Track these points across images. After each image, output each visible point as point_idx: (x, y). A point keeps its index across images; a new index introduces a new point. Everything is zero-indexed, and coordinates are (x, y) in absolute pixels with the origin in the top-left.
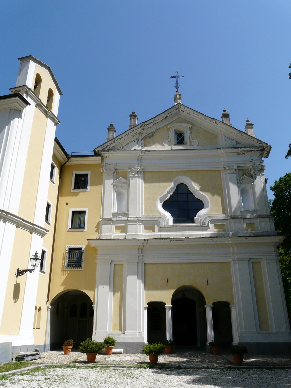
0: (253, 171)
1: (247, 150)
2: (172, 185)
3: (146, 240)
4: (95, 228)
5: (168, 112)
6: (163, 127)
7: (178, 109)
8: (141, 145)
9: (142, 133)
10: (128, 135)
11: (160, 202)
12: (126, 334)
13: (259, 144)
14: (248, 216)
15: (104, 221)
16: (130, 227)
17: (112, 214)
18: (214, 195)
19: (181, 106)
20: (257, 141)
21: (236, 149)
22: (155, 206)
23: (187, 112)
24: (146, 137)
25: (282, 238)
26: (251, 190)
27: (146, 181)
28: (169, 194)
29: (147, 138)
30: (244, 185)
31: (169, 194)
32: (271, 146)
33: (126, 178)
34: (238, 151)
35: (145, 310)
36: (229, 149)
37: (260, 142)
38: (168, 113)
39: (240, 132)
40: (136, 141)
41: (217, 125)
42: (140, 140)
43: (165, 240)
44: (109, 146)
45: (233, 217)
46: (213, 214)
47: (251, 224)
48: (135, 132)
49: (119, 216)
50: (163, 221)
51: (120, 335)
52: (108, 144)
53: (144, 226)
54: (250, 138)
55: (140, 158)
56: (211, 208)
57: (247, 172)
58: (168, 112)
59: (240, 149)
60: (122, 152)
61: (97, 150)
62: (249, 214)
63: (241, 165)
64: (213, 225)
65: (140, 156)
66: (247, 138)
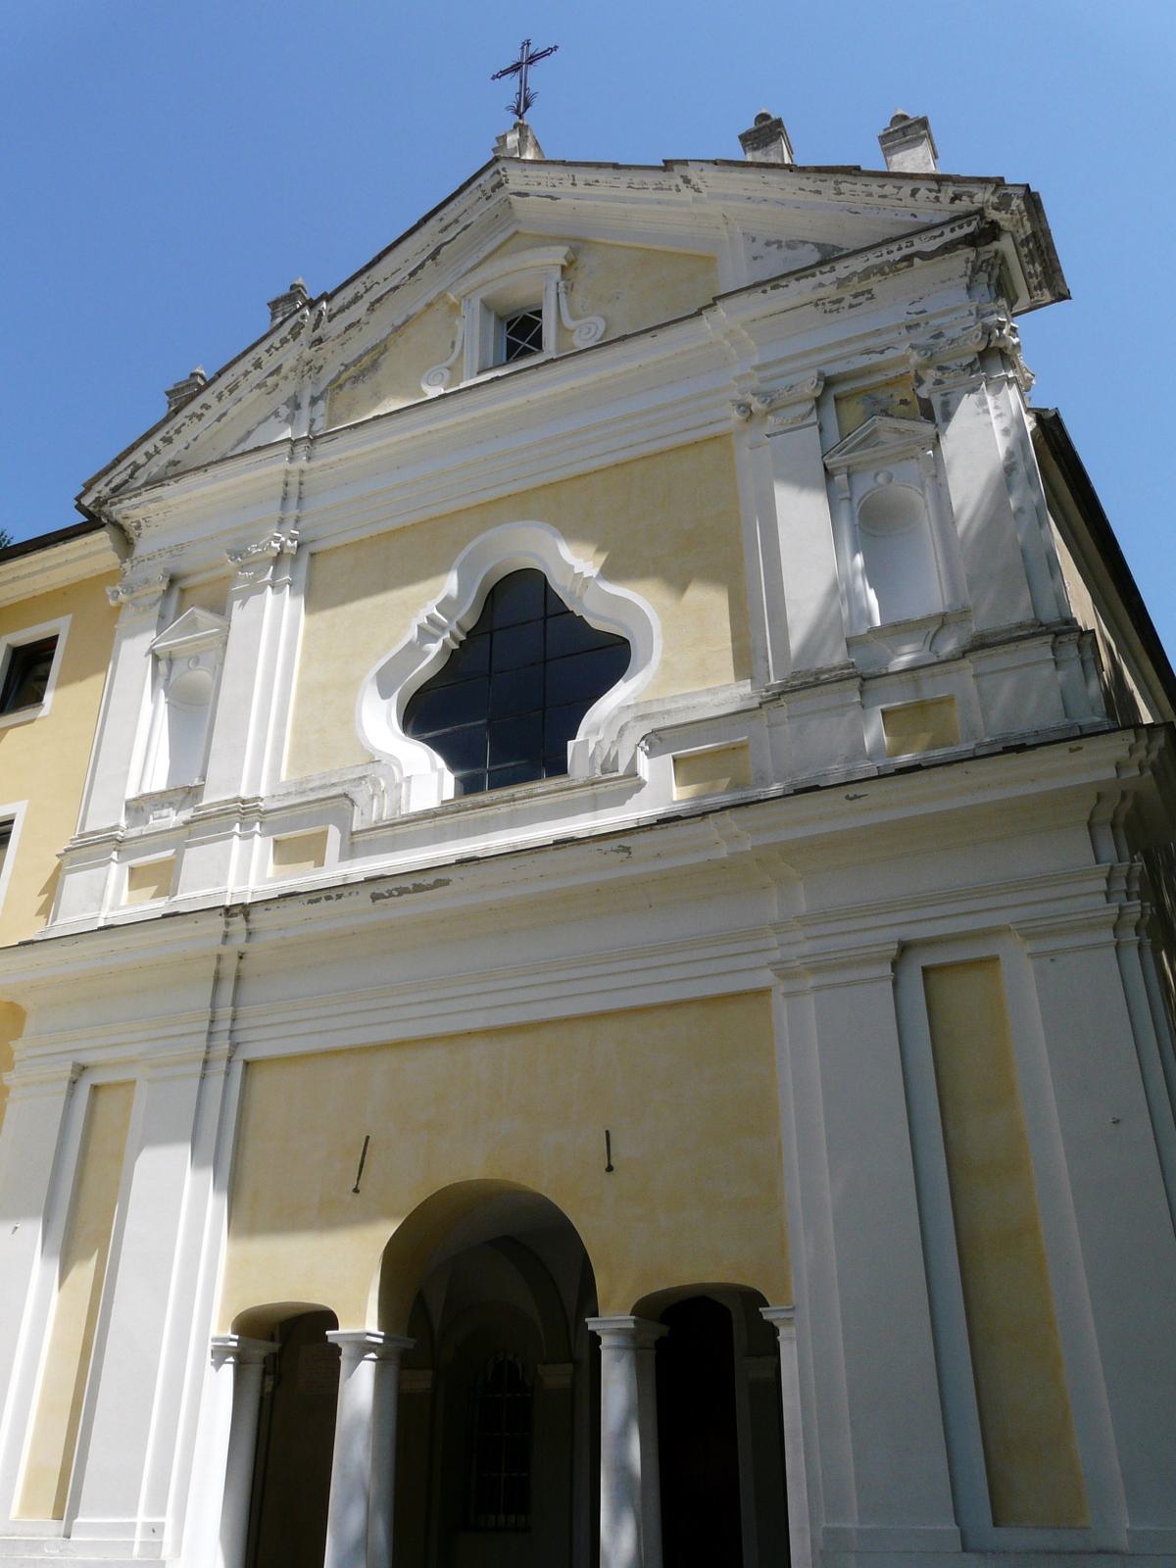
0: (931, 375)
1: (875, 266)
2: (450, 584)
3: (236, 911)
4: (40, 894)
5: (441, 220)
6: (429, 305)
7: (493, 190)
8: (311, 426)
9: (321, 367)
10: (236, 386)
11: (379, 697)
12: (72, 1538)
13: (953, 200)
14: (903, 659)
15: (91, 848)
16: (196, 859)
17: (127, 808)
18: (682, 588)
19: (509, 172)
20: (934, 186)
21: (807, 277)
22: (348, 719)
23: (544, 189)
24: (340, 381)
25: (1131, 750)
26: (923, 496)
27: (316, 599)
28: (435, 642)
29: (348, 385)
30: (877, 475)
31: (435, 639)
32: (1028, 186)
33: (220, 608)
34: (821, 285)
35: (218, 1364)
36: (764, 292)
37: (950, 190)
38: (446, 228)
39: (824, 176)
40: (284, 411)
41: (698, 190)
42: (305, 401)
43: (339, 897)
44: (143, 465)
45: (804, 683)
46: (673, 698)
47: (922, 707)
48: (269, 364)
49: (157, 813)
50: (372, 797)
51: (35, 1546)
52: (138, 456)
53: (276, 842)
54: (889, 189)
55: (293, 489)
56: (665, 663)
57: (897, 399)
58: (441, 220)
59: (833, 269)
60: (201, 476)
61: (87, 501)
62: (907, 648)
63: (852, 367)
64: (667, 760)
65: (290, 479)
66: (875, 200)
